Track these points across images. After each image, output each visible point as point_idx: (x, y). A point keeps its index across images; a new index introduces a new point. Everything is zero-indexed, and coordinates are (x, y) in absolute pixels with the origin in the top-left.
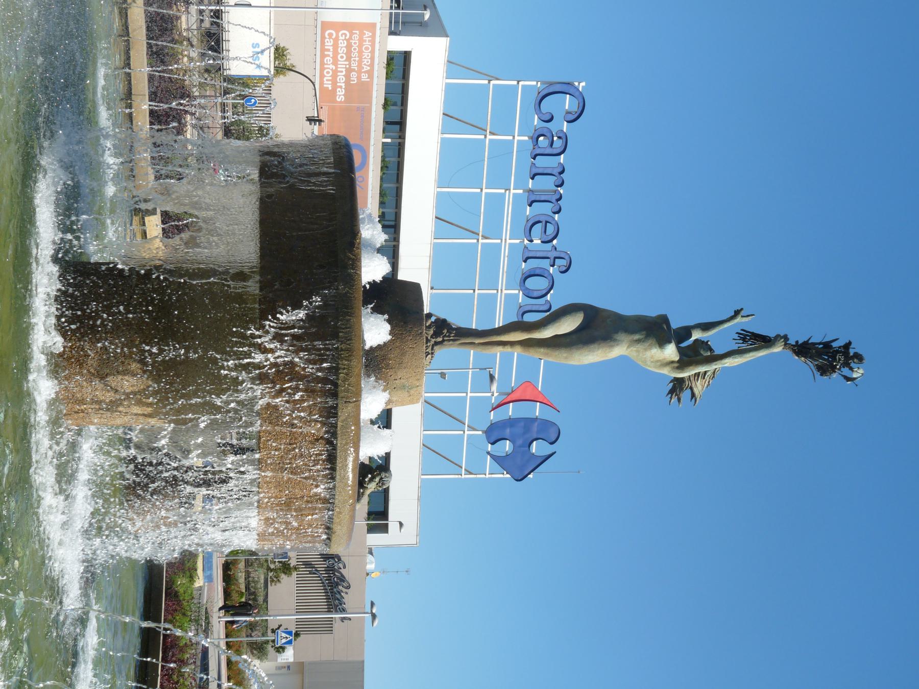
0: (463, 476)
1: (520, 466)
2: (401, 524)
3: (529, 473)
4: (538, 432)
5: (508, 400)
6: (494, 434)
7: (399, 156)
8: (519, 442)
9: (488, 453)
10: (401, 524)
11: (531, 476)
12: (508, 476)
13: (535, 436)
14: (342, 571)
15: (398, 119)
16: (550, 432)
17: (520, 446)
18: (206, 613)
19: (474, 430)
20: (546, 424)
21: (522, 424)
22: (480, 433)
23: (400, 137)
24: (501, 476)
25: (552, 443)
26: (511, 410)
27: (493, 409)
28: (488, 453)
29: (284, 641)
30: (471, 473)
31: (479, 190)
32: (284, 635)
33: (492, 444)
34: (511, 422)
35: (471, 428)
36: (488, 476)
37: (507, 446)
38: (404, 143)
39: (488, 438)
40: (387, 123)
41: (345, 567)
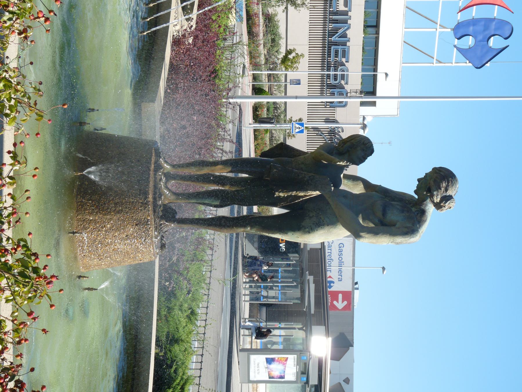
0: (435, 65)
1: (480, 57)
2: (387, 75)
3: (487, 63)
4: (496, 29)
5: (472, 4)
6: (460, 31)
7: (377, 8)
8: (480, 37)
9: (455, 46)
10: (387, 75)
11: (488, 65)
12: (470, 64)
13: (493, 33)
14: (341, 134)
15: (372, 90)
16: (505, 30)
17: (481, 41)
18: (240, 109)
19: (444, 28)
20: (502, 23)
21: (483, 23)
22: (449, 30)
23: (376, 34)
24: (465, 64)
25: (506, 39)
26: (474, 12)
27: (460, 11)
28: (455, 46)
29: (297, 130)
30: (440, 62)
31: (435, 30)
32: (297, 126)
33: (459, 39)
34: (474, 22)
35: (442, 26)
36: (454, 64)
37: (470, 41)
38: (379, 37)
39: (455, 34)
40: (366, 26)
41: (343, 131)
